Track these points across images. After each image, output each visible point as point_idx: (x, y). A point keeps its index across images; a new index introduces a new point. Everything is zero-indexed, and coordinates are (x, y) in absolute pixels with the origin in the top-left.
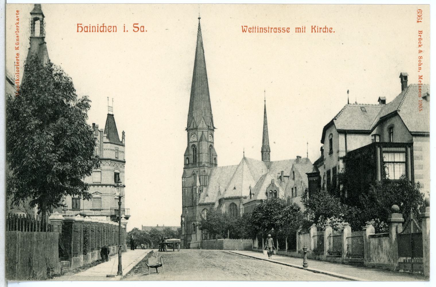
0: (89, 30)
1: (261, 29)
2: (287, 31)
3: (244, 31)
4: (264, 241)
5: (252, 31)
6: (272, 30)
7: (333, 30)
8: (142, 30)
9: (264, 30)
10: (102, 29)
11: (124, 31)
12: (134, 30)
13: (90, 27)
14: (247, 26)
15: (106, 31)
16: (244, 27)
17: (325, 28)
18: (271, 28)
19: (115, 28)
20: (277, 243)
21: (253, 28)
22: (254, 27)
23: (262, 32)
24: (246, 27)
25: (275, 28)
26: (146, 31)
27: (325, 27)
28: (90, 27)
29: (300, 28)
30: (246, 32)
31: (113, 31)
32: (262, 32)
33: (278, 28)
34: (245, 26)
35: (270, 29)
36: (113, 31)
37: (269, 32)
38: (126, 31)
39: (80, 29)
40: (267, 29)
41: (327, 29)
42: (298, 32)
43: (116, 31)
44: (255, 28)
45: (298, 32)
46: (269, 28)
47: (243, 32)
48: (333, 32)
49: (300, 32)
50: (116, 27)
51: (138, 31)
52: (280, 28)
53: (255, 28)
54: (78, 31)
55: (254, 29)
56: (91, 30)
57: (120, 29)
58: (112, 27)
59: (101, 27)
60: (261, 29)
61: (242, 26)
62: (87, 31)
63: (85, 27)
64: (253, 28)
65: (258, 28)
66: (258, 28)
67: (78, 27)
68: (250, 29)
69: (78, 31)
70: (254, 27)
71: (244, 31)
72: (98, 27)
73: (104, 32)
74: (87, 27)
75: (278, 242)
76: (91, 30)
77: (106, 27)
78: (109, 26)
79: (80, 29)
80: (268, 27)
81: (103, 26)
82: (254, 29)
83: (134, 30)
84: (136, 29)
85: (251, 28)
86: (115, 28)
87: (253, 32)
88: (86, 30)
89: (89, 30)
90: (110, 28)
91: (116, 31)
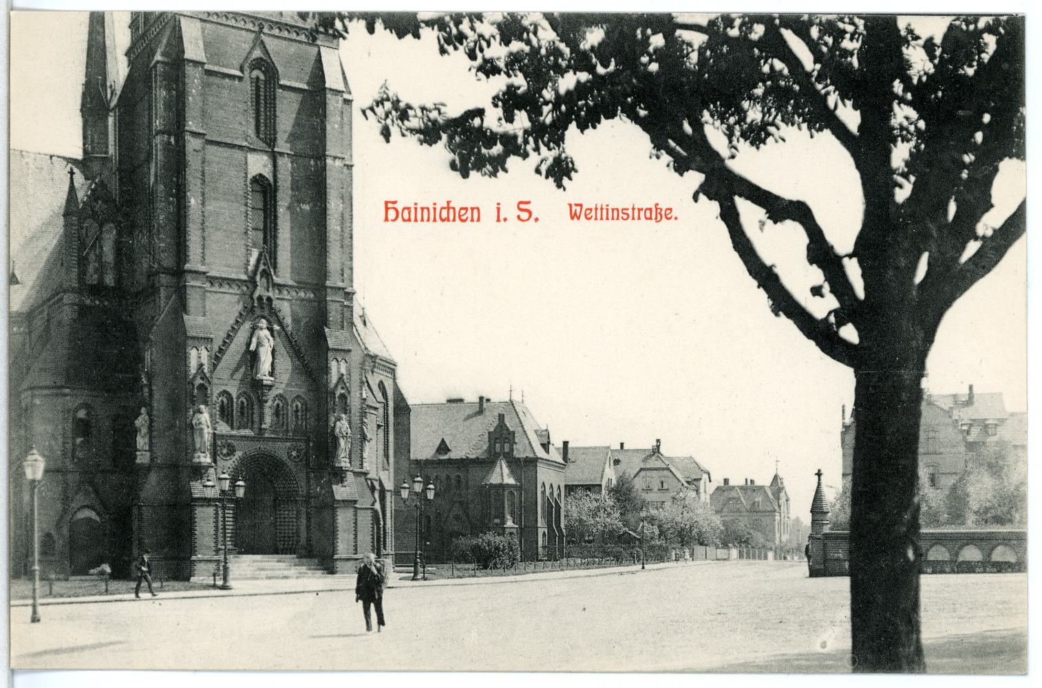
0: (413, 218)
1: (615, 212)
2: (666, 215)
3: (574, 216)
4: (679, 153)
5: (594, 217)
6: (642, 213)
7: (674, 214)
8: (406, 217)
9: (621, 215)
10: (444, 214)
11: (498, 220)
12: (519, 217)
13: (416, 209)
14: (581, 205)
15: (454, 220)
16: (574, 208)
17: (448, 208)
18: (640, 210)
19: (475, 211)
20: (682, 151)
21: (596, 209)
22: (599, 207)
23: (618, 219)
24: (578, 208)
25: (647, 209)
26: (676, 218)
27: (446, 205)
28: (416, 209)
29: (428, 209)
30: (578, 218)
31: (472, 220)
32: (618, 219)
33: (623, 209)
34: (576, 205)
35: (636, 211)
36: (472, 220)
37: (633, 219)
38: (501, 218)
39: (392, 214)
40: (630, 212)
41: (451, 211)
42: (422, 220)
43: (478, 220)
44: (602, 209)
45: (422, 220)
46: (633, 209)
47: (572, 218)
48: (673, 218)
49: (428, 220)
50: (478, 209)
51: (528, 220)
52: (627, 209)
53: (602, 209)
54: (386, 219)
55: (599, 211)
56: (419, 218)
57: (488, 213)
58: (469, 211)
59: (442, 208)
60: (615, 212)
61: (570, 205)
62: (409, 220)
63: (404, 209)
64: (596, 209)
65: (607, 209)
66: (607, 209)
67: (387, 209)
68: (588, 212)
69: (386, 219)
70: (599, 207)
71: (574, 216)
72: (435, 209)
73: (448, 220)
74: (409, 209)
75: (681, 154)
76: (419, 218)
77: (454, 208)
78: (667, 209)
79: (392, 214)
80: (630, 207)
81: (448, 208)
82: (599, 211)
83: (519, 217)
84: (525, 215)
85: (591, 210)
86: (475, 211)
87: (596, 219)
88: (406, 217)
89: (413, 218)
90: (463, 212)
91: (478, 220)
